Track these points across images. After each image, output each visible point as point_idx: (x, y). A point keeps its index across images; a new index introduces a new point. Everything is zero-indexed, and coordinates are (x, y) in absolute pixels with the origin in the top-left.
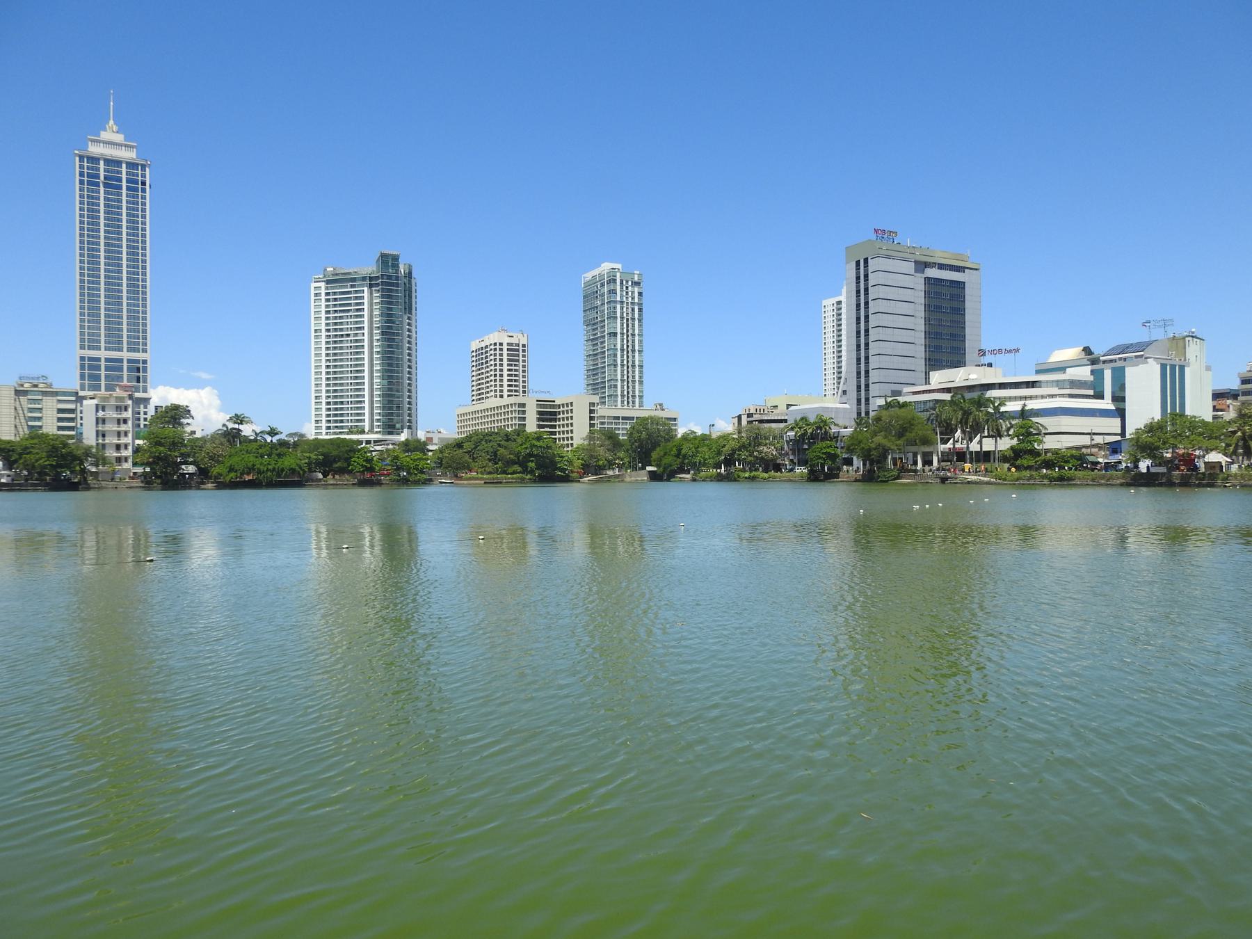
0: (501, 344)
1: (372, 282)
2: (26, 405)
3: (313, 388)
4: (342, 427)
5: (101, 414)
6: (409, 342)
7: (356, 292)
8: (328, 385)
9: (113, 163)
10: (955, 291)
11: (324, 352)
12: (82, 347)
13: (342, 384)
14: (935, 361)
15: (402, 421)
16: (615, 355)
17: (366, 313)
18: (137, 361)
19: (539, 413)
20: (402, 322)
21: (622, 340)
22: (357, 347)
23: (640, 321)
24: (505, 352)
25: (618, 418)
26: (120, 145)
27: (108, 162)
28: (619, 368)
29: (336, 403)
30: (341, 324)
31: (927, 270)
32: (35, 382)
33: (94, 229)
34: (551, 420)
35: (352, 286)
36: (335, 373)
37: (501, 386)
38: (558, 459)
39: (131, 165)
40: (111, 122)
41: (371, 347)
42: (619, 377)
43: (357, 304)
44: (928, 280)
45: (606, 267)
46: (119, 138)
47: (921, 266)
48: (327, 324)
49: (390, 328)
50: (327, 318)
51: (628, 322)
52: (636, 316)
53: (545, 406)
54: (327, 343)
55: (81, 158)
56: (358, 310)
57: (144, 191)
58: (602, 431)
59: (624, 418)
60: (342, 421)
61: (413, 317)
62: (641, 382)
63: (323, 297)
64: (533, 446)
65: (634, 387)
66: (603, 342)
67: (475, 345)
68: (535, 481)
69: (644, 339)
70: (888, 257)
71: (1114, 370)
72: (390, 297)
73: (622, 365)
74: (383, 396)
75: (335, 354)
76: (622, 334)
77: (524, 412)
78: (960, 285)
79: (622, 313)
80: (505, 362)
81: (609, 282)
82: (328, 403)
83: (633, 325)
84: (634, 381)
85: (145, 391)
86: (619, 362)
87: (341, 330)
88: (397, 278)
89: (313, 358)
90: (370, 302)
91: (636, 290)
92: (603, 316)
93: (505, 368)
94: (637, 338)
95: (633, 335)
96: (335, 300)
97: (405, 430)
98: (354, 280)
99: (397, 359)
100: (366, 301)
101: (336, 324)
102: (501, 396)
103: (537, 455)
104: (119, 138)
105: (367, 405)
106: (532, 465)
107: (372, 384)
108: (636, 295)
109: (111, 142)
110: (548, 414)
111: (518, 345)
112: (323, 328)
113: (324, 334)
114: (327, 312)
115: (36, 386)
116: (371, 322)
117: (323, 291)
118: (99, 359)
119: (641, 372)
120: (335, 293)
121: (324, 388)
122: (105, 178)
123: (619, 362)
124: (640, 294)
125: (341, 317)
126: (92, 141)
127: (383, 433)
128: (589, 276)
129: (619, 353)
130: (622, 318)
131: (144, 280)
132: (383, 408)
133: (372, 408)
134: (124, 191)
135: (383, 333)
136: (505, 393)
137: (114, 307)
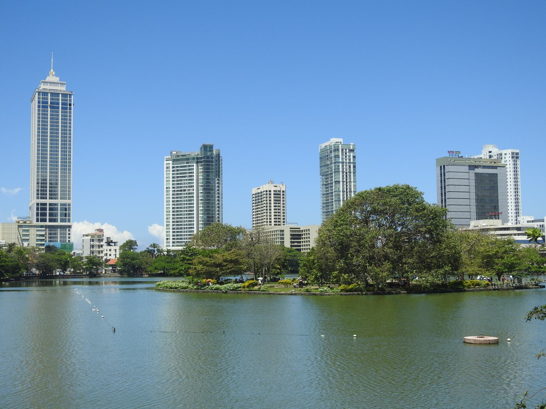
0: (270, 191)
1: (198, 160)
2: (22, 233)
3: (165, 220)
4: (181, 242)
5: (92, 243)
6: (218, 193)
7: (189, 166)
8: (173, 218)
9: (55, 94)
11: (171, 200)
12: (38, 198)
13: (181, 218)
14: (481, 216)
16: (339, 195)
17: (195, 178)
18: (65, 205)
19: (291, 235)
20: (214, 183)
21: (343, 185)
22: (190, 197)
23: (354, 173)
24: (272, 196)
27: (52, 94)
29: (178, 228)
30: (181, 184)
31: (476, 169)
32: (25, 220)
33: (44, 133)
34: (298, 239)
35: (187, 163)
36: (177, 211)
37: (270, 216)
39: (64, 95)
40: (52, 70)
41: (198, 197)
44: (477, 174)
45: (333, 140)
46: (56, 79)
47: (472, 167)
48: (173, 184)
50: (173, 181)
51: (346, 174)
52: (352, 170)
53: (295, 231)
54: (173, 194)
55: (39, 93)
56: (190, 176)
57: (70, 109)
60: (181, 239)
63: (171, 169)
66: (332, 187)
67: (255, 191)
69: (357, 184)
70: (454, 165)
75: (177, 201)
76: (343, 182)
77: (283, 235)
79: (343, 169)
80: (272, 202)
81: (335, 150)
82: (173, 229)
83: (350, 176)
85: (69, 221)
87: (181, 187)
88: (212, 158)
89: (165, 203)
90: (197, 171)
91: (352, 154)
92: (331, 170)
93: (273, 205)
94: (352, 184)
95: (350, 182)
96: (178, 170)
98: (188, 159)
99: (212, 204)
100: (195, 171)
101: (178, 184)
102: (270, 225)
104: (56, 79)
107: (198, 218)
108: (352, 157)
109: (52, 82)
110: (296, 236)
111: (280, 191)
112: (171, 186)
113: (171, 189)
114: (173, 177)
115: (25, 222)
116: (198, 183)
117: (171, 166)
118: (46, 204)
120: (177, 167)
122: (51, 103)
123: (341, 199)
124: (354, 157)
125: (180, 180)
126: (43, 82)
128: (323, 146)
130: (343, 172)
131: (70, 159)
135: (204, 189)
136: (273, 223)
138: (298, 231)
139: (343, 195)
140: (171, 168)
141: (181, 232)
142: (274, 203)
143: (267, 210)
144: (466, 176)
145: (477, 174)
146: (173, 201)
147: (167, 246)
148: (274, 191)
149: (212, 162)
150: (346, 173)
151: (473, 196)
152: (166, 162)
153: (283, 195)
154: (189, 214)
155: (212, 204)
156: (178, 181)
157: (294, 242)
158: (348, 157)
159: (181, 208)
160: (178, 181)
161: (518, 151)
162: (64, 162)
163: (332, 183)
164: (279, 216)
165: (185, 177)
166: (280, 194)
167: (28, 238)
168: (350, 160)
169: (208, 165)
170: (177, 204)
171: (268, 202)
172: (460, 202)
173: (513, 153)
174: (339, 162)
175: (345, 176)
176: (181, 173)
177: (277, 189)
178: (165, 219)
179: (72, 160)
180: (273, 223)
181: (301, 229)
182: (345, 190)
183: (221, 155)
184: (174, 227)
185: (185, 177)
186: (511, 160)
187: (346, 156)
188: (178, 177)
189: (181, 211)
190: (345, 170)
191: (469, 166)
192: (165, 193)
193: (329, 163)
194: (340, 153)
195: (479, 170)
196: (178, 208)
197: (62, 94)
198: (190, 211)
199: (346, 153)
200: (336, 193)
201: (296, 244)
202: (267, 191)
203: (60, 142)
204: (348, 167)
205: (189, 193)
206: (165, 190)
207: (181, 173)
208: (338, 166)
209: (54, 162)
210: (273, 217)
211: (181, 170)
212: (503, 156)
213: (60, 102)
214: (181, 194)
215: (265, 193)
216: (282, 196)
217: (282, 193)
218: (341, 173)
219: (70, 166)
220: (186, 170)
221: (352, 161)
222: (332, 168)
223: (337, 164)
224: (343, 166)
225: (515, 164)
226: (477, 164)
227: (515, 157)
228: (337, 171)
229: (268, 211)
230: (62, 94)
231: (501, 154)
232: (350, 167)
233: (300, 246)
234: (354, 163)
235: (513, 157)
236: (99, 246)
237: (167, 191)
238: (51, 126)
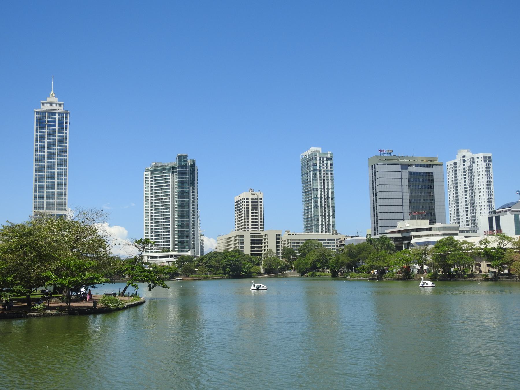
0: (247, 199)
1: (173, 170)
3: (145, 228)
7: (166, 176)
8: (152, 226)
9: (52, 114)
10: (429, 177)
15: (189, 244)
16: (317, 201)
19: (252, 240)
21: (321, 192)
23: (332, 180)
24: (250, 203)
25: (325, 240)
27: (49, 113)
28: (319, 209)
30: (158, 193)
33: (42, 149)
34: (258, 244)
35: (164, 173)
36: (155, 219)
37: (248, 222)
38: (243, 266)
39: (61, 114)
40: (52, 92)
42: (320, 214)
43: (166, 182)
45: (312, 149)
46: (55, 100)
47: (404, 166)
48: (152, 194)
49: (183, 194)
50: (152, 190)
51: (324, 182)
52: (330, 178)
53: (256, 236)
54: (152, 203)
55: (37, 112)
57: (66, 126)
58: (285, 249)
59: (328, 240)
61: (196, 188)
62: (333, 217)
64: (228, 260)
65: (329, 220)
66: (311, 194)
67: (236, 199)
68: (229, 278)
69: (335, 190)
71: (496, 217)
72: (183, 178)
73: (321, 207)
74: (179, 231)
75: (155, 209)
76: (321, 189)
77: (243, 240)
78: (430, 174)
79: (320, 177)
80: (250, 209)
83: (328, 183)
84: (329, 216)
86: (319, 205)
89: (145, 212)
90: (172, 179)
91: (329, 162)
92: (310, 178)
93: (250, 212)
94: (330, 191)
95: (328, 189)
96: (156, 180)
97: (191, 250)
98: (165, 169)
100: (170, 180)
101: (156, 193)
103: (231, 265)
104: (55, 100)
105: (171, 236)
106: (228, 270)
107: (173, 225)
108: (329, 165)
109: (52, 103)
111: (257, 199)
112: (150, 195)
113: (150, 199)
114: (152, 187)
117: (150, 176)
119: (333, 211)
120: (155, 177)
121: (150, 228)
122: (48, 122)
123: (319, 205)
124: (332, 165)
125: (158, 190)
127: (179, 251)
129: (319, 200)
130: (321, 179)
131: (66, 172)
132: (179, 238)
133: (173, 238)
134: (57, 127)
135: (178, 198)
137: (50, 177)
138: (259, 236)
139: (321, 202)
140: (150, 178)
143: (245, 225)
144: (398, 175)
148: (252, 199)
150: (324, 180)
151: (406, 196)
155: (186, 211)
156: (156, 190)
157: (254, 247)
158: (325, 165)
159: (158, 216)
160: (156, 190)
161: (490, 155)
164: (256, 222)
165: (162, 186)
166: (257, 202)
168: (327, 168)
170: (155, 213)
172: (392, 202)
173: (485, 157)
174: (316, 170)
175: (323, 184)
176: (159, 183)
177: (255, 196)
178: (144, 226)
179: (67, 174)
182: (323, 196)
183: (196, 165)
185: (162, 186)
186: (484, 164)
187: (323, 164)
188: (156, 187)
189: (158, 219)
190: (322, 177)
191: (401, 165)
192: (145, 202)
194: (318, 162)
195: (411, 169)
196: (156, 216)
197: (59, 113)
199: (323, 161)
201: (256, 249)
202: (244, 199)
203: (56, 157)
204: (325, 174)
205: (166, 202)
206: (145, 199)
207: (159, 183)
208: (316, 174)
209: (51, 175)
210: (250, 224)
212: (476, 160)
213: (57, 120)
214: (158, 203)
215: (243, 200)
216: (259, 203)
217: (259, 200)
218: (319, 181)
219: (65, 179)
220: (162, 180)
221: (329, 168)
223: (315, 172)
224: (320, 174)
225: (488, 168)
226: (412, 162)
227: (488, 160)
228: (315, 179)
230: (59, 113)
231: (473, 158)
232: (327, 174)
233: (261, 251)
234: (332, 171)
235: (485, 161)
237: (146, 200)
238: (48, 142)
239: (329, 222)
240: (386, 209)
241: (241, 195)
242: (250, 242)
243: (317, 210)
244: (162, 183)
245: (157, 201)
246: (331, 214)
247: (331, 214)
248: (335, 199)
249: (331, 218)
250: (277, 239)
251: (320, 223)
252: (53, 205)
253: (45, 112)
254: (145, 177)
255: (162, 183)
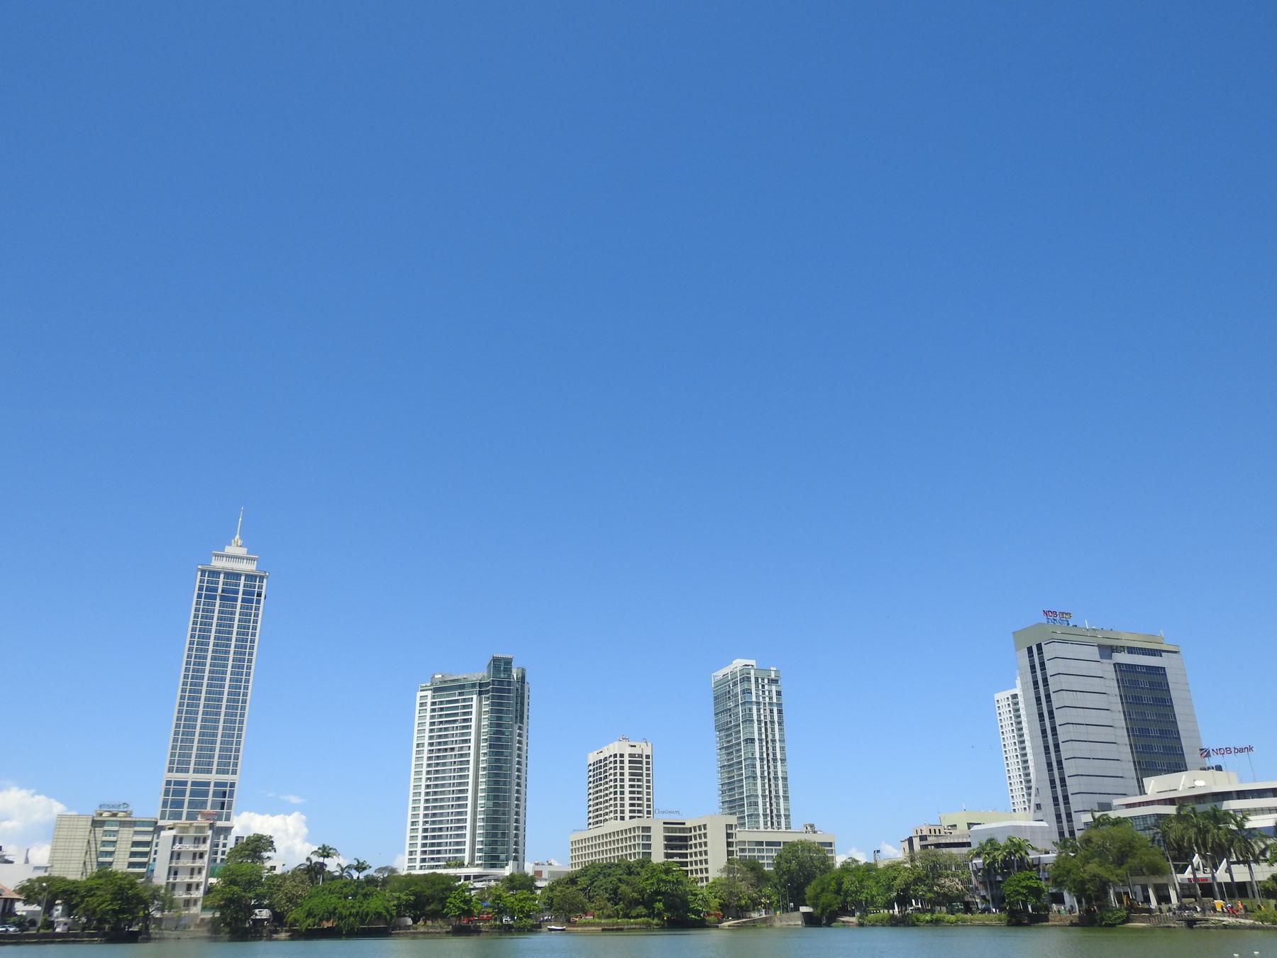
0: (622, 756)
1: (481, 688)
3: (410, 812)
4: (439, 860)
5: (177, 847)
7: (464, 700)
11: (425, 769)
13: (441, 807)
14: (1147, 765)
15: (508, 850)
16: (754, 766)
18: (224, 785)
19: (667, 838)
20: (512, 733)
21: (761, 748)
24: (627, 765)
26: (243, 558)
28: (759, 781)
30: (446, 736)
32: (115, 810)
34: (681, 847)
35: (460, 694)
37: (622, 805)
39: (250, 577)
42: (760, 793)
44: (1118, 666)
45: (738, 663)
46: (242, 552)
47: (1107, 651)
51: (767, 725)
52: (776, 719)
54: (430, 758)
55: (203, 572)
56: (465, 720)
57: (258, 602)
59: (769, 844)
60: (439, 852)
62: (786, 798)
63: (429, 707)
65: (778, 804)
67: (593, 757)
68: (662, 927)
69: (786, 745)
70: (1064, 642)
72: (500, 704)
73: (763, 778)
74: (487, 820)
75: (437, 772)
76: (761, 740)
77: (649, 838)
79: (759, 716)
80: (627, 777)
81: (742, 680)
83: (773, 730)
86: (759, 774)
87: (446, 743)
88: (509, 683)
89: (413, 776)
90: (478, 709)
91: (774, 688)
92: (737, 719)
93: (627, 783)
94: (778, 745)
95: (774, 741)
96: (442, 709)
97: (511, 863)
98: (463, 687)
99: (505, 776)
100: (474, 710)
101: (440, 737)
102: (622, 818)
104: (242, 552)
106: (659, 905)
109: (235, 556)
110: (678, 840)
111: (640, 756)
112: (426, 741)
113: (426, 748)
115: (115, 815)
117: (429, 701)
118: (185, 783)
119: (785, 786)
120: (441, 703)
123: (759, 774)
124: (779, 693)
125: (446, 729)
126: (216, 555)
127: (485, 866)
128: (719, 674)
129: (758, 763)
130: (759, 721)
132: (487, 835)
135: (490, 746)
136: (627, 815)
139: (762, 767)
141: (440, 837)
142: (631, 792)
143: (616, 812)
144: (1095, 669)
145: (1118, 666)
146: (428, 772)
147: (410, 868)
148: (631, 755)
149: (509, 691)
152: (420, 694)
153: (648, 763)
154: (459, 799)
160: (440, 730)
162: (233, 701)
163: (739, 744)
165: (455, 721)
166: (641, 762)
167: (111, 849)
168: (771, 698)
169: (501, 697)
170: (436, 779)
171: (618, 777)
172: (1094, 733)
176: (447, 715)
177: (636, 751)
180: (627, 815)
181: (688, 825)
183: (527, 680)
184: (427, 826)
185: (455, 721)
188: (441, 723)
191: (1099, 646)
193: (732, 705)
196: (436, 786)
198: (460, 791)
200: (749, 762)
202: (615, 756)
205: (461, 755)
206: (415, 749)
207: (447, 715)
208: (750, 710)
209: (214, 697)
211: (448, 709)
213: (241, 589)
214: (445, 757)
221: (775, 700)
222: (737, 714)
223: (748, 706)
224: (759, 710)
229: (618, 796)
232: (771, 711)
234: (779, 705)
236: (195, 854)
239: (778, 810)
240: (1084, 749)
241: (605, 749)
242: (663, 842)
243: (755, 784)
244: (456, 714)
245: (442, 752)
246: (781, 793)
247: (781, 793)
248: (788, 763)
249: (781, 800)
250: (729, 836)
251: (761, 812)
252: (211, 764)
253: (219, 573)
254: (418, 702)
255: (456, 714)
